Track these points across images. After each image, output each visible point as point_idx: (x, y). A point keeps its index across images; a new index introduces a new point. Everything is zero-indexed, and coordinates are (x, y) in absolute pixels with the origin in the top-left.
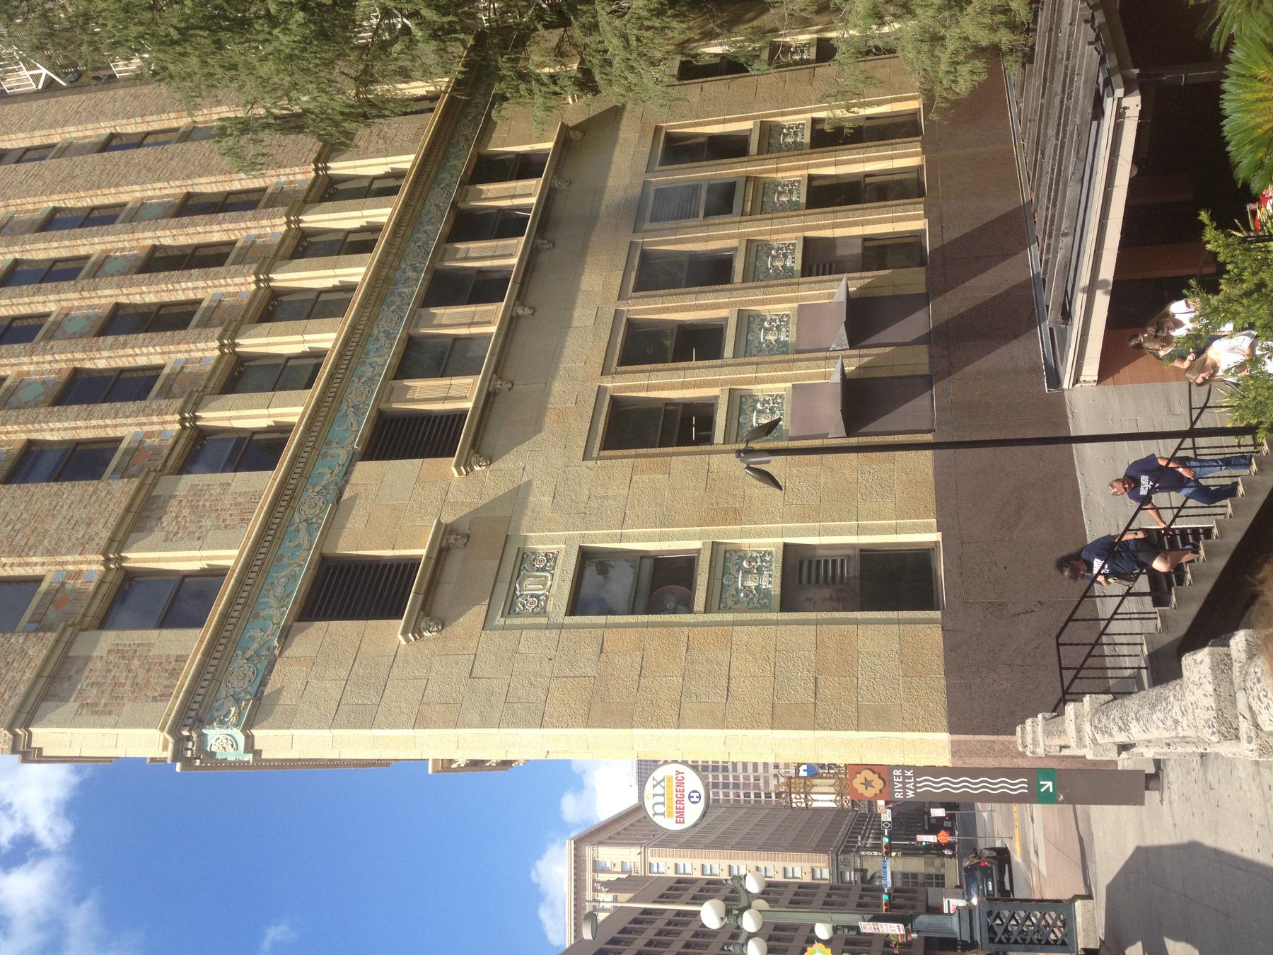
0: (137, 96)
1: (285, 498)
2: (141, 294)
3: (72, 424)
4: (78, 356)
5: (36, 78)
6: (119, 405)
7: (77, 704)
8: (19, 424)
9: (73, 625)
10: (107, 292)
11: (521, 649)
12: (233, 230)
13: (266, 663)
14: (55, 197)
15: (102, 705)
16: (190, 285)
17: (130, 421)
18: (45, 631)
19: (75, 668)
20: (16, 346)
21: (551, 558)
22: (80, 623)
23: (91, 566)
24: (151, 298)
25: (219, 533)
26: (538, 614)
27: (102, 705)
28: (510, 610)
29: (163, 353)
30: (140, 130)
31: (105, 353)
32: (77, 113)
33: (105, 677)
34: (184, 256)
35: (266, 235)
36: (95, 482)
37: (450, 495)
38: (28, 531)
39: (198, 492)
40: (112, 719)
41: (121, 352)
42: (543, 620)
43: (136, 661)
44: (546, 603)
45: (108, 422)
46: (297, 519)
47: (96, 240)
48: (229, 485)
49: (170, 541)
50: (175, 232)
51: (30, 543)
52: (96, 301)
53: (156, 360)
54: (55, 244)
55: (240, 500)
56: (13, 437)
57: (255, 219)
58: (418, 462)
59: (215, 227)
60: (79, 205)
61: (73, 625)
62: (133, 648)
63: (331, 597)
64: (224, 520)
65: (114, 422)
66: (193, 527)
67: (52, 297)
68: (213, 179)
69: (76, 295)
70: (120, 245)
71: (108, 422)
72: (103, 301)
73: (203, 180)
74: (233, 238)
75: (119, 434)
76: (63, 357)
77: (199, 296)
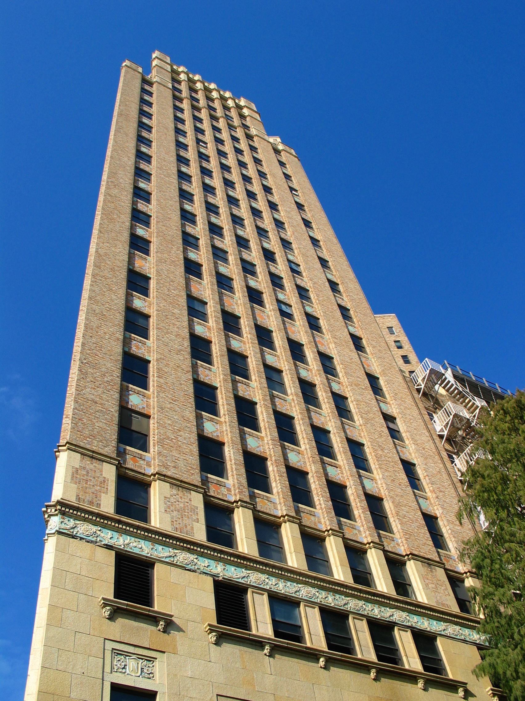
0: (440, 472)
1: (188, 545)
2: (314, 482)
3: (233, 458)
4: (273, 458)
5: (442, 430)
6: (245, 476)
7: (78, 467)
8: (231, 438)
9: (119, 463)
10: (313, 467)
11: (91, 658)
12: (361, 519)
13: (93, 539)
14: (369, 444)
15: (77, 476)
16: (322, 502)
17: (236, 481)
18: (117, 454)
19: (96, 465)
20: (277, 434)
21: (151, 676)
22: (207, 495)
23: (402, 550)
24: (313, 486)
25: (169, 519)
26: (112, 668)
27: (77, 476)
28: (116, 652)
29: (278, 493)
30: (420, 476)
31: (275, 469)
32: (424, 449)
33: (91, 476)
34: (436, 530)
35: (361, 535)
36: (199, 468)
37: (192, 623)
38: (172, 445)
39: (194, 510)
40: (69, 480)
41: (277, 475)
42: (108, 669)
43: (99, 488)
44: (120, 672)
45: (235, 472)
46: (300, 586)
47: (345, 461)
48: (198, 522)
49: (423, 578)
50: (355, 493)
51: (164, 445)
52: (308, 464)
53: (275, 491)
54: (340, 445)
55: (189, 527)
56: (225, 437)
57: (369, 528)
58: (214, 607)
59: (360, 511)
60: (368, 454)
61: (119, 463)
62: (106, 487)
63: (226, 594)
64: (176, 521)
65: (234, 474)
66: (172, 508)
67: (308, 446)
68: (392, 509)
69: (310, 455)
70: (344, 472)
71: (235, 472)
72: (309, 467)
73: (391, 504)
74: (357, 520)
75: (229, 478)
76: (272, 453)
77: (317, 507)
